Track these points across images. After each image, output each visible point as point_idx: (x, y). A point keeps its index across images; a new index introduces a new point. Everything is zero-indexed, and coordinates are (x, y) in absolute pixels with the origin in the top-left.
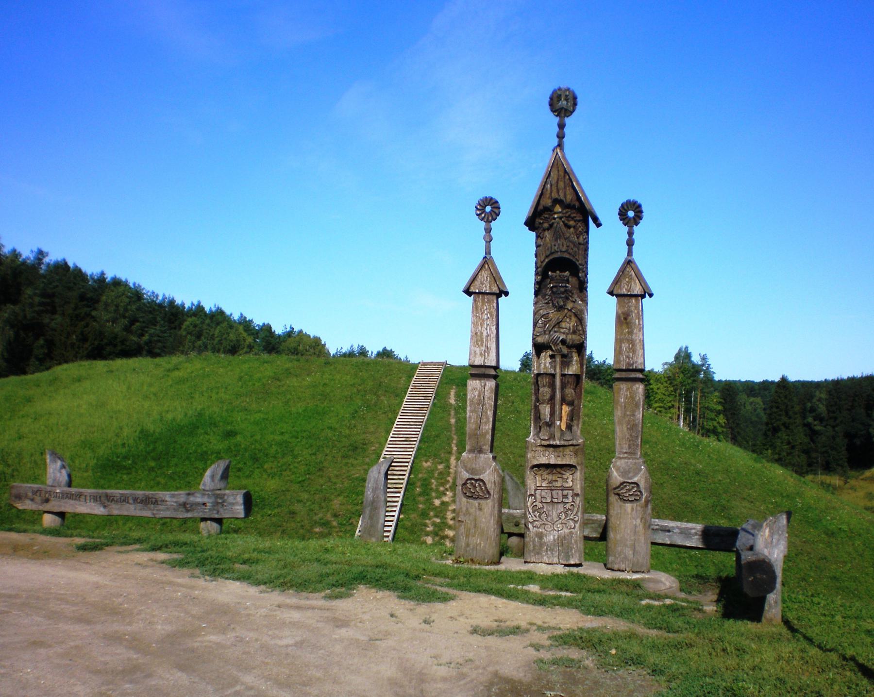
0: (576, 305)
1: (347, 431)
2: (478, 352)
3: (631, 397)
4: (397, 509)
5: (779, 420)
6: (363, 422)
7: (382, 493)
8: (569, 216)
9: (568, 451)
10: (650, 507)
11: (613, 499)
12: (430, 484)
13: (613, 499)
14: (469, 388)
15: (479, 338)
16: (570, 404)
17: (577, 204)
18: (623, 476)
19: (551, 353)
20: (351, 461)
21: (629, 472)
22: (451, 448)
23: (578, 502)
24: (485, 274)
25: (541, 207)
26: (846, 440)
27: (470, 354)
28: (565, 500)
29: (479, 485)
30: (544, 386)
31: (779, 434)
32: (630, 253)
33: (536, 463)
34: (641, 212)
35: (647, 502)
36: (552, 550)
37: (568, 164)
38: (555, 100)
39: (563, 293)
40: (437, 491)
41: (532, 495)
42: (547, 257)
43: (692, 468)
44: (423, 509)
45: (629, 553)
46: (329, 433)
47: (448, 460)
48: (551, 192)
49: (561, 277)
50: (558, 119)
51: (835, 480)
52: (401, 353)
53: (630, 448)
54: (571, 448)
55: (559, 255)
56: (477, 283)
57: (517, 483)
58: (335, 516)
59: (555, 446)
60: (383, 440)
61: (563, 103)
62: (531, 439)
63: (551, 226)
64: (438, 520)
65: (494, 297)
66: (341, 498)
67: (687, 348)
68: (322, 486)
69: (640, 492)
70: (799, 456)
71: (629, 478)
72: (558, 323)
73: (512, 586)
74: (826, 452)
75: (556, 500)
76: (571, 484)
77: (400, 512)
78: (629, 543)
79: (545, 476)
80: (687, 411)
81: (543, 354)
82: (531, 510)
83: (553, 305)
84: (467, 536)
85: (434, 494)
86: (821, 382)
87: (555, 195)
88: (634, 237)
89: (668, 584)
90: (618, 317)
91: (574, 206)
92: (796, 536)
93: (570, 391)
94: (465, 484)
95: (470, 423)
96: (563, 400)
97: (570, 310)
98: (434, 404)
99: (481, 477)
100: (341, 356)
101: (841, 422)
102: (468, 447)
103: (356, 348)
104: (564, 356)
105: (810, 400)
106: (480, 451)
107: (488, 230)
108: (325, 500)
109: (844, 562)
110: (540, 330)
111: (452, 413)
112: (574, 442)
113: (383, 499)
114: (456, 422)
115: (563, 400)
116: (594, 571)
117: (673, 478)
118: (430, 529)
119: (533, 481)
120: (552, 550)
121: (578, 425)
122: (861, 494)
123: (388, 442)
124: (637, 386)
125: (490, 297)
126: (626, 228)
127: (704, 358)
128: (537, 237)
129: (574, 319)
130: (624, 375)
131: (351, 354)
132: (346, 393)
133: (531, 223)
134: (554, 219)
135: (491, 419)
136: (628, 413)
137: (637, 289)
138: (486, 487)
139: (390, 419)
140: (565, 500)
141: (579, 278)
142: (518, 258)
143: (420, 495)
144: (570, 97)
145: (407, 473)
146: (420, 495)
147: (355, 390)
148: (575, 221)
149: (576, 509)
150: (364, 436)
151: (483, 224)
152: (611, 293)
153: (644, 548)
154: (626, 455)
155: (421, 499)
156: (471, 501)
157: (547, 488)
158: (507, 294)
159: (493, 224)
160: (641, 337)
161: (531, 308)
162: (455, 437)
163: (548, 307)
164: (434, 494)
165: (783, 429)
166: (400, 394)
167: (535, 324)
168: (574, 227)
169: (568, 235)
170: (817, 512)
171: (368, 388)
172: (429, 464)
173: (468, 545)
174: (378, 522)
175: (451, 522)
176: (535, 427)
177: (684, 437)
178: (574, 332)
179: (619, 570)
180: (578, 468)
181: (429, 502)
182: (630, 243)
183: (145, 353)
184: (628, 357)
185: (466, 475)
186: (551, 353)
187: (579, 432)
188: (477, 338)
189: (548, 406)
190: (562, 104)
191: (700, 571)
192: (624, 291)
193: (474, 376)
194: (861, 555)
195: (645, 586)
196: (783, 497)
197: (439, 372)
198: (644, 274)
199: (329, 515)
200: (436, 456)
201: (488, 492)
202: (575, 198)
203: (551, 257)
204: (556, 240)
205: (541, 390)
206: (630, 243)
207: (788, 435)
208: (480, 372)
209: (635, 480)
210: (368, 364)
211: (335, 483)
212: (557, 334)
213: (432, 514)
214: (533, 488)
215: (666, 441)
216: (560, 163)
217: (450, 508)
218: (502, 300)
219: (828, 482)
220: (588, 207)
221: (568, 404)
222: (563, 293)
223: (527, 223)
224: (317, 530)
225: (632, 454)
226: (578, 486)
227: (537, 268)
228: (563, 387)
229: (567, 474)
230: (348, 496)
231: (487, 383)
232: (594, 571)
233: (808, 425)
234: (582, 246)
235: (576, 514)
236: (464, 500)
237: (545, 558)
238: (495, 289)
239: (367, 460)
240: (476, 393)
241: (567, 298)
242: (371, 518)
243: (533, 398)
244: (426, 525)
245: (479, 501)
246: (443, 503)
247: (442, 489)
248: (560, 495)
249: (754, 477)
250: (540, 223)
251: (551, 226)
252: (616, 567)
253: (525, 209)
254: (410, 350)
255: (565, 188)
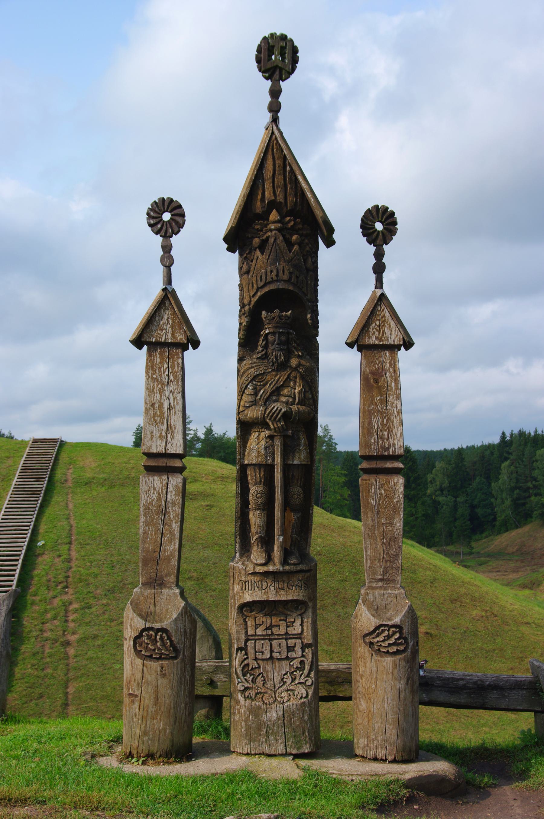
2: (156, 433)
15: (157, 412)
24: (167, 315)
28: (291, 654)
29: (162, 638)
50: (269, 83)
54: (300, 576)
69: (405, 639)
71: (390, 620)
82: (239, 672)
86: (440, 451)
126: (373, 249)
130: (372, 465)
134: (271, 230)
135: (177, 535)
138: (171, 641)
140: (291, 654)
142: (214, 290)
154: (380, 584)
157: (264, 637)
158: (196, 344)
159: (174, 240)
160: (399, 405)
179: (375, 759)
183: (438, 476)
218: (190, 354)
227: (242, 306)
235: (308, 676)
237: (265, 746)
238: (181, 337)
240: (155, 496)
253: (224, 217)
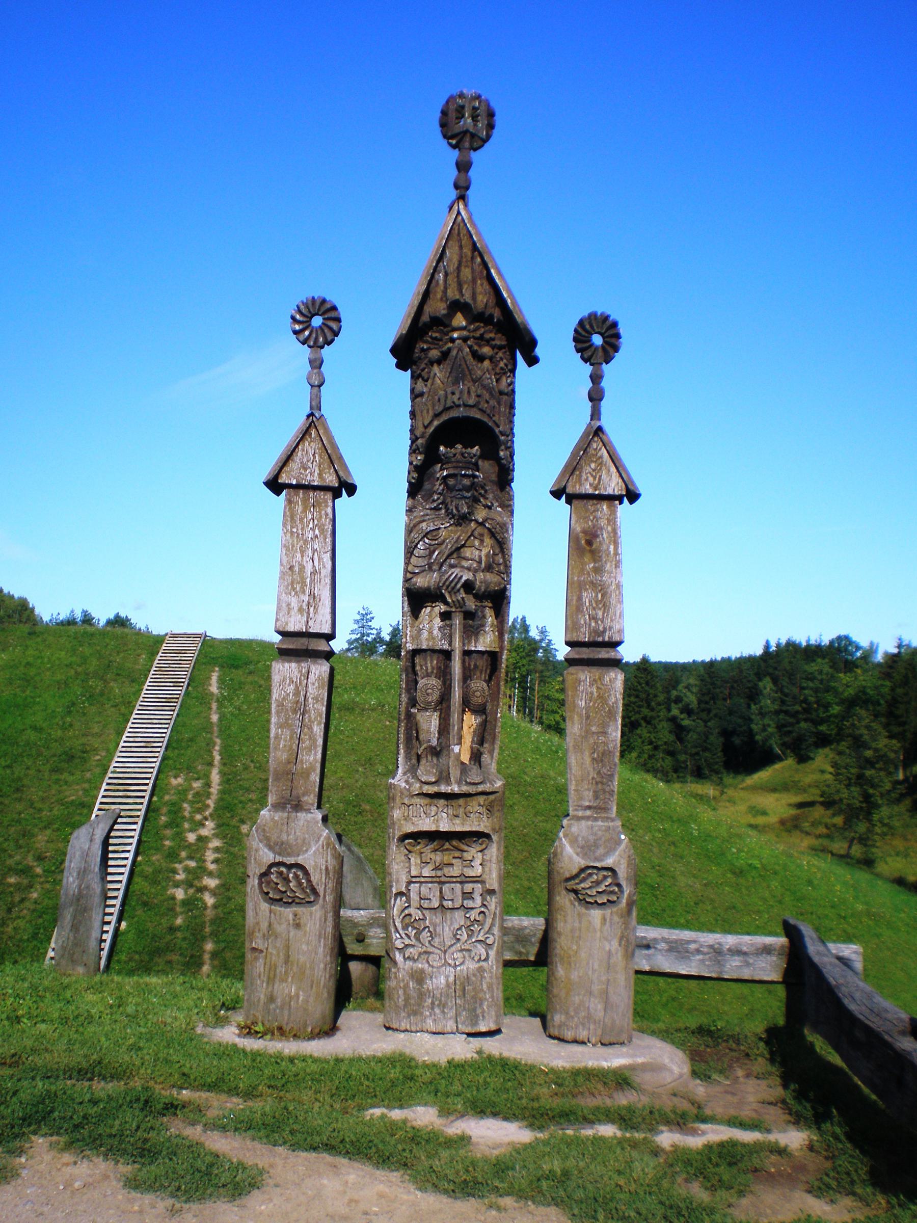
0: (492, 514)
1: (59, 733)
3: (599, 697)
4: (132, 848)
5: (639, 712)
6: (83, 719)
7: (97, 879)
8: (481, 337)
9: (475, 805)
10: (634, 914)
11: (564, 899)
12: (181, 809)
13: (564, 899)
14: (276, 678)
16: (480, 710)
17: (497, 314)
18: (585, 855)
19: (443, 608)
20: (65, 776)
21: (596, 845)
22: (212, 758)
23: (492, 907)
24: (310, 447)
25: (425, 318)
26: (722, 740)
27: (279, 608)
28: (468, 903)
29: (296, 876)
30: (428, 675)
31: (638, 731)
32: (596, 414)
33: (410, 829)
34: (618, 336)
35: (630, 904)
36: (443, 1006)
37: (479, 234)
38: (452, 115)
39: (468, 489)
40: (191, 820)
41: (401, 894)
42: (436, 416)
43: (552, 782)
44: (170, 847)
45: (596, 1006)
46: (32, 735)
47: (207, 776)
48: (446, 288)
49: (462, 457)
50: (456, 153)
51: (708, 789)
52: (140, 621)
53: (596, 797)
54: (481, 799)
55: (461, 412)
56: (294, 465)
57: (358, 858)
58: (40, 858)
59: (450, 797)
60: (111, 746)
61: (467, 122)
62: (399, 780)
63: (445, 355)
64: (192, 864)
65: (329, 496)
66: (48, 832)
67: (524, 619)
68: (20, 814)
69: (619, 885)
70: (663, 760)
72: (458, 549)
73: (377, 1112)
74: (697, 754)
75: (449, 904)
76: (478, 870)
77: (137, 854)
78: (596, 988)
79: (428, 854)
80: (524, 699)
81: (426, 611)
83: (449, 513)
84: (271, 980)
85: (186, 825)
86: (688, 663)
87: (453, 294)
88: (604, 384)
89: (676, 1070)
90: (573, 538)
91: (491, 316)
92: (694, 876)
93: (479, 685)
94: (266, 874)
95: (276, 748)
96: (466, 704)
97: (482, 524)
98: (187, 693)
99: (300, 860)
100: (57, 624)
101: (716, 715)
102: (271, 799)
103: (78, 616)
104: (469, 615)
105: (674, 688)
106: (298, 807)
107: (317, 364)
108: (24, 836)
109: (759, 911)
110: (422, 562)
111: (214, 706)
112: (487, 787)
113: (98, 890)
114: (220, 720)
115: (466, 704)
116: (523, 1044)
117: (526, 798)
118: (181, 877)
119: (402, 867)
120: (443, 1006)
121: (491, 752)
122: (742, 808)
123: (120, 749)
124: (613, 675)
125: (321, 495)
126: (588, 369)
127: (543, 632)
128: (414, 378)
129: (488, 541)
131: (71, 622)
132: (59, 677)
133: (405, 352)
134: (453, 340)
135: (320, 741)
136: (594, 729)
137: (613, 486)
138: (309, 881)
139: (124, 715)
140: (468, 903)
141: (498, 460)
143: (167, 826)
144: (482, 111)
145: (147, 795)
146: (167, 826)
147: (73, 672)
148: (493, 347)
149: (489, 921)
150: (84, 740)
151: (306, 351)
152: (557, 494)
153: (623, 994)
154: (588, 813)
155: (168, 832)
156: (277, 908)
157: (432, 880)
158: (351, 489)
161: (402, 520)
162: (218, 741)
163: (438, 516)
164: (186, 825)
165: (644, 724)
166: (138, 679)
167: (409, 552)
168: (491, 359)
169: (479, 373)
170: (718, 841)
171: (91, 669)
172: (180, 780)
173: (271, 999)
174: (88, 937)
175: (212, 867)
176: (408, 757)
177: (537, 739)
178: (489, 568)
179: (575, 1041)
180: (495, 838)
181: (179, 836)
182: (596, 397)
184: (593, 618)
185: (269, 857)
186: (443, 608)
187: (494, 767)
188: (294, 578)
189: (436, 715)
190: (466, 128)
191: (704, 1020)
192: (587, 489)
193: (285, 654)
194: (780, 902)
195: (638, 1080)
196: (673, 822)
197: (194, 649)
198: (622, 457)
199: (30, 858)
200: (189, 769)
201: (314, 891)
202: (492, 302)
203: (445, 417)
204: (456, 382)
205: (422, 682)
206: (596, 397)
207: (649, 732)
208: (302, 646)
209: (609, 862)
210: (92, 635)
211: (40, 810)
212: (456, 571)
213: (183, 854)
214: (404, 878)
215: (514, 745)
216: (464, 232)
217: (211, 845)
218: (344, 501)
219: (700, 792)
220: (519, 320)
221: (474, 712)
222: (468, 489)
223: (394, 351)
224: (12, 880)
225: (600, 809)
226: (494, 875)
228: (467, 676)
229: (472, 851)
230: (58, 829)
231: (313, 668)
232: (523, 1044)
233: (673, 719)
234: (505, 398)
236: (265, 906)
237: (430, 1022)
238: (331, 480)
239: (88, 775)
241: (476, 500)
242: (75, 928)
243: (404, 698)
244: (175, 872)
245: (295, 909)
246: (201, 839)
247: (198, 817)
248: (459, 893)
249: (634, 795)
250: (423, 350)
251: (445, 355)
252: (569, 1035)
254: (151, 619)
255: (474, 281)
